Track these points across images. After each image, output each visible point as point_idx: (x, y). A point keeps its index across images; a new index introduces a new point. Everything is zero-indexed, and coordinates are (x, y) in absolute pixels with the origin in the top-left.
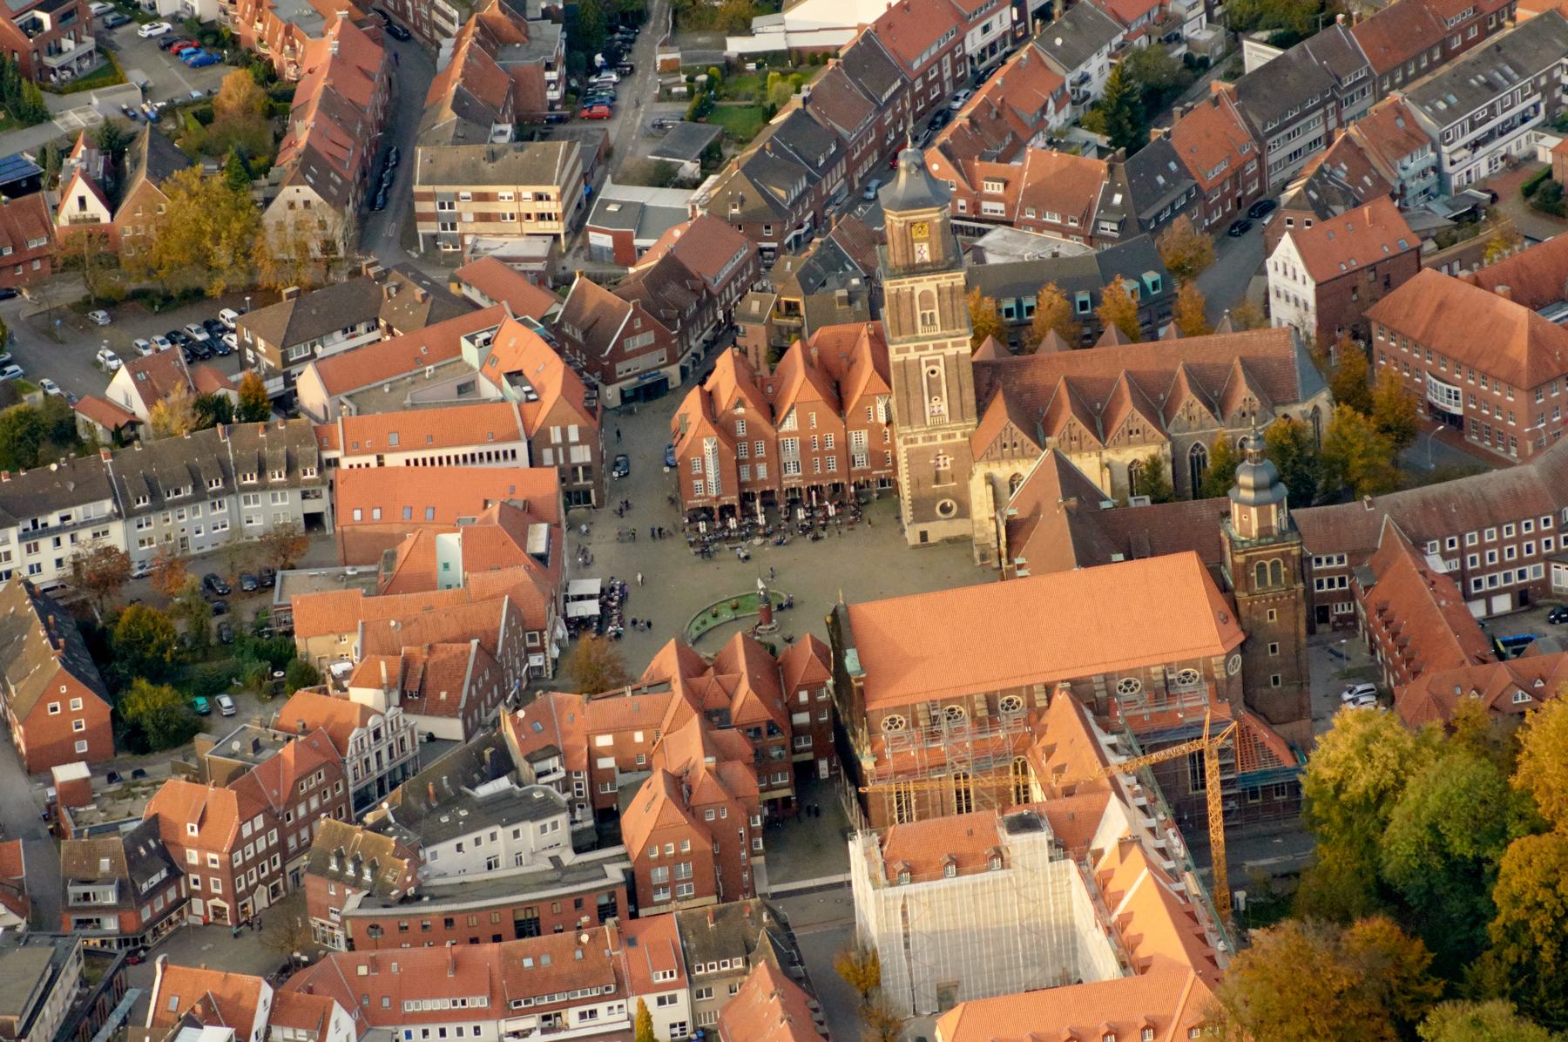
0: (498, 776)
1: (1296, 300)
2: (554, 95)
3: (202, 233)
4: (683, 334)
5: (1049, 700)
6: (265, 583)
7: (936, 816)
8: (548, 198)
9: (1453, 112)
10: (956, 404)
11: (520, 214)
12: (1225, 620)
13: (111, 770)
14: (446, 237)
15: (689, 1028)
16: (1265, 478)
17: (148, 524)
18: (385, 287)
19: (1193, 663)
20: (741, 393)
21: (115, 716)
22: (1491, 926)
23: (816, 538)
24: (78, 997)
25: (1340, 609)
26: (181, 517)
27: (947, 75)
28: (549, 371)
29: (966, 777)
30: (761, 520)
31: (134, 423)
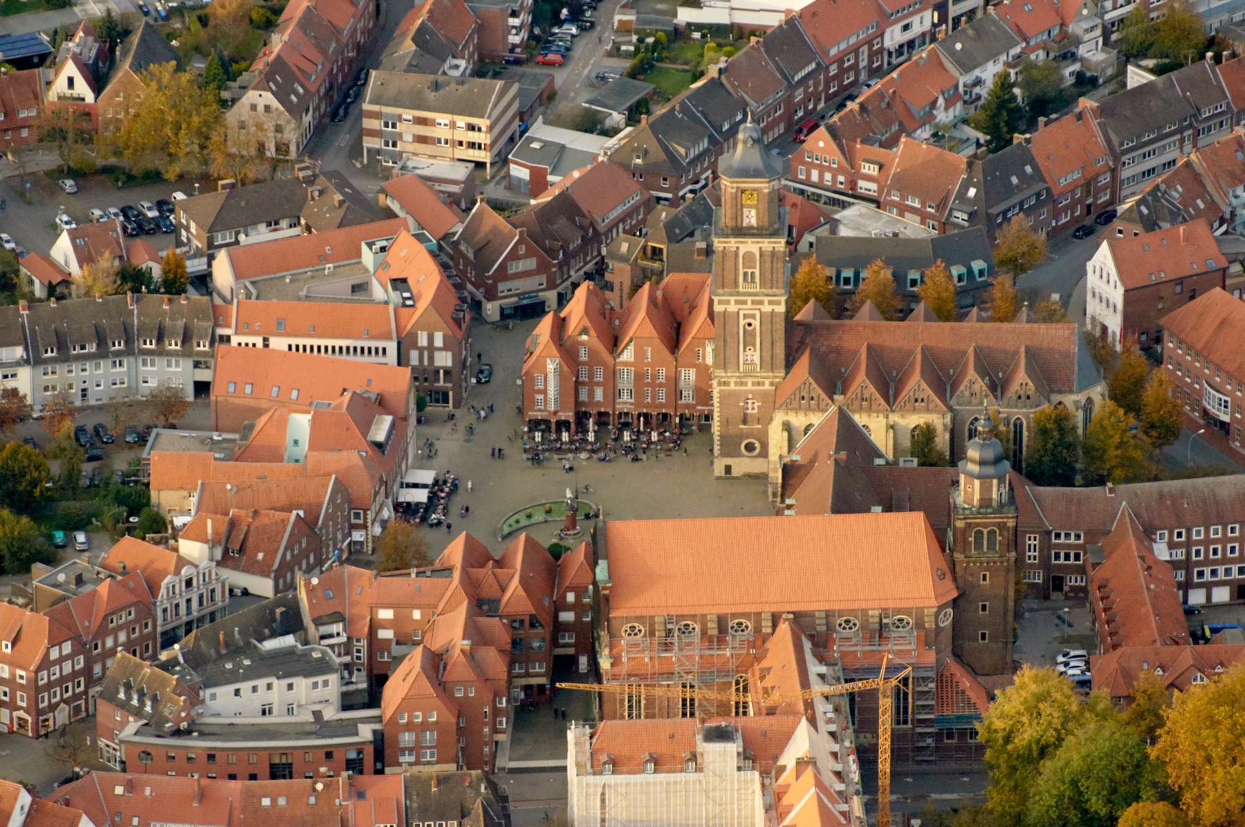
1: (1108, 301)
2: (514, 39)
3: (164, 122)
4: (563, 265)
8: (480, 130)
10: (767, 356)
11: (453, 141)
12: (942, 577)
14: (387, 152)
16: (990, 454)
18: (310, 190)
19: (907, 611)
23: (636, 459)
25: (1073, 581)
26: (70, 371)
30: (591, 437)
31: (67, 282)
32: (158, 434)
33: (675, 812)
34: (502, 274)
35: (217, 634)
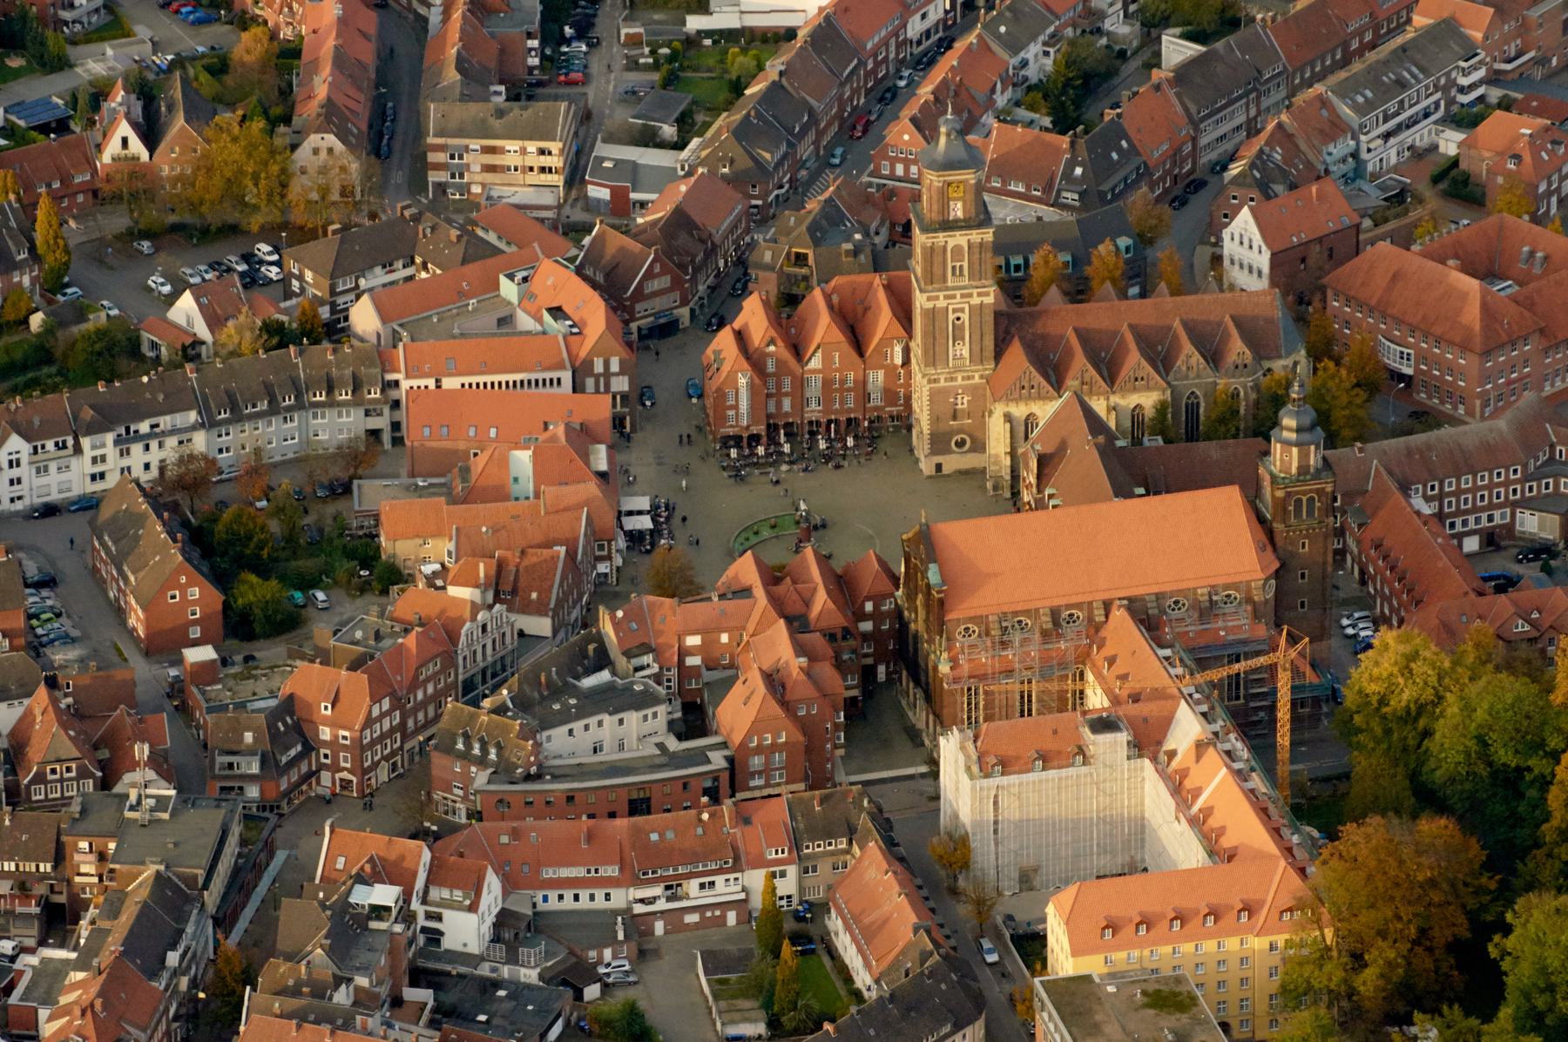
0: (599, 668)
4: (694, 280)
5: (1107, 616)
7: (1000, 719)
8: (550, 153)
9: (1370, 106)
10: (977, 348)
11: (524, 167)
15: (795, 900)
16: (1307, 421)
17: (228, 434)
18: (421, 228)
19: (1235, 586)
20: (773, 333)
21: (226, 606)
22: (1544, 827)
23: (838, 467)
24: (240, 855)
26: (257, 429)
27: (892, 56)
28: (593, 312)
29: (1030, 682)
30: (787, 448)
32: (359, 486)
33: (1066, 806)
34: (639, 295)
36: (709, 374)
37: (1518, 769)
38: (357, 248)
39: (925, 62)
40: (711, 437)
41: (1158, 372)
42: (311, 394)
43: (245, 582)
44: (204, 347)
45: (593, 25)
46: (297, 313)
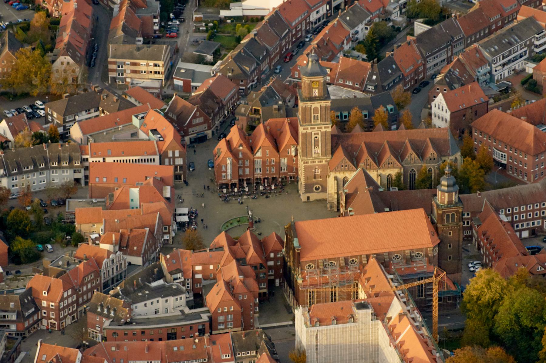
0: (159, 279)
3: (31, 72)
4: (213, 119)
5: (368, 261)
6: (62, 203)
7: (323, 303)
8: (159, 66)
9: (497, 52)
10: (324, 150)
11: (148, 71)
12: (433, 235)
13: (8, 270)
14: (119, 78)
16: (451, 182)
17: (16, 179)
18: (102, 96)
19: (421, 250)
20: (241, 142)
21: (9, 250)
22: (540, 352)
23: (267, 197)
24: (5, 354)
26: (28, 177)
27: (304, 28)
29: (335, 288)
30: (246, 189)
31: (8, 141)
32: (69, 201)
33: (346, 340)
34: (190, 125)
35: (133, 282)
36: (215, 158)
37: (532, 328)
38: (75, 103)
39: (317, 31)
40: (216, 184)
41: (398, 161)
42: (51, 163)
43: (17, 240)
44: (10, 143)
45: (182, 13)
46: (49, 130)
